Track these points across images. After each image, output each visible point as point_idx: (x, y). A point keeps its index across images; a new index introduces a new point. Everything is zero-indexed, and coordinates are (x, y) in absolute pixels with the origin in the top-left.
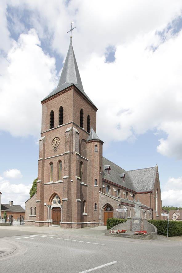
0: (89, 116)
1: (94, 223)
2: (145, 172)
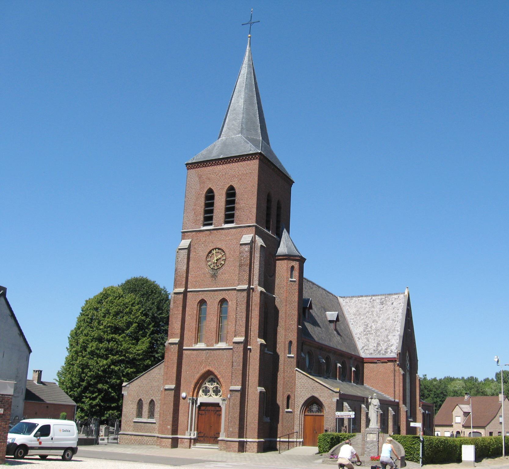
0: (279, 203)
1: (287, 440)
2: (382, 303)
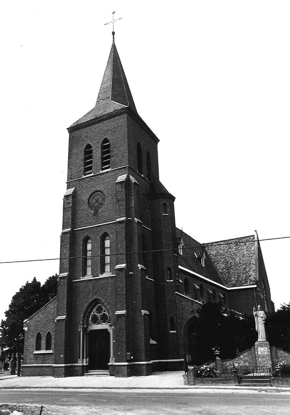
0: (148, 153)
